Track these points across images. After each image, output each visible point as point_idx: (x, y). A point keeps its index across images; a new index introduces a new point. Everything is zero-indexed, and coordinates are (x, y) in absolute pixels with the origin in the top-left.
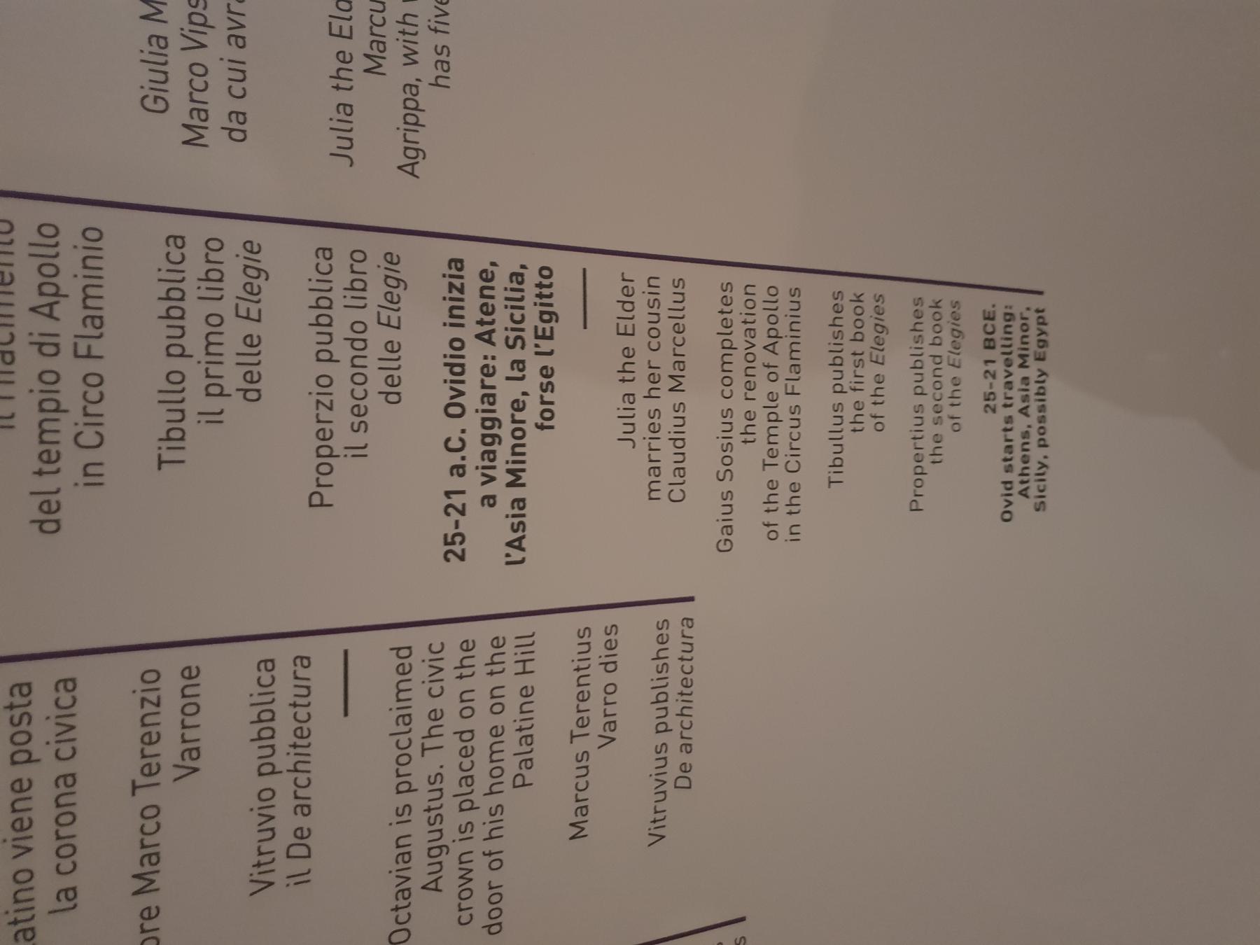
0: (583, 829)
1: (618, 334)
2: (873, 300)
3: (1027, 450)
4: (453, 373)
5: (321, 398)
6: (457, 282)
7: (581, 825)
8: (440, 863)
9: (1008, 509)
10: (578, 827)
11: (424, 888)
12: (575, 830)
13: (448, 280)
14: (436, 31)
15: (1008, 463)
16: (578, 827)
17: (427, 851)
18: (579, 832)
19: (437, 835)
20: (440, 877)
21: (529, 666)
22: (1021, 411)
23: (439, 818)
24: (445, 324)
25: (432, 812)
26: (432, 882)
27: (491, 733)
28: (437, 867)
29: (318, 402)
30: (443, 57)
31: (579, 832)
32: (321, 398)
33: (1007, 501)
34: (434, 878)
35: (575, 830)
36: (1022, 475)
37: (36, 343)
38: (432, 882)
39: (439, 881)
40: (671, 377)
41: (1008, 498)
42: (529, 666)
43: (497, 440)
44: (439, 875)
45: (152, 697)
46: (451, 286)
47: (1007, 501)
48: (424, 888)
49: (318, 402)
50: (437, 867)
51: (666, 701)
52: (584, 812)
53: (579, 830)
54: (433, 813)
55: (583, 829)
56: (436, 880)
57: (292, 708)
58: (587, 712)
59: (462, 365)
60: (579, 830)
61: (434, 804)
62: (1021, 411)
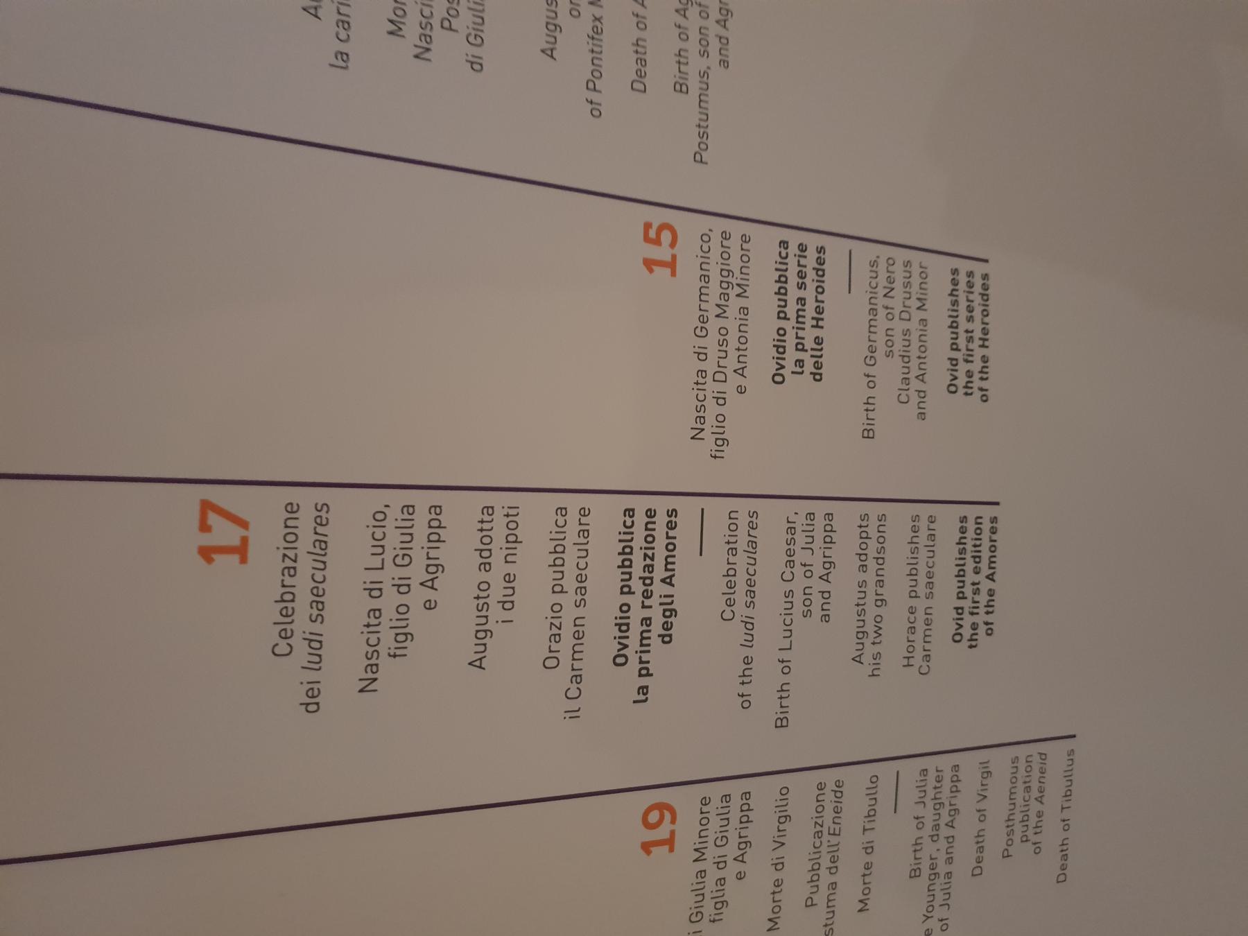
0: (704, 854)
1: (829, 834)
2: (902, 266)
3: (981, 523)
4: (620, 631)
5: (287, 552)
6: (650, 553)
7: (702, 850)
8: (485, 645)
9: (953, 382)
10: (700, 852)
11: (422, 584)
12: (697, 855)
13: (643, 551)
14: (715, 457)
15: (970, 335)
16: (700, 852)
17: (475, 633)
18: (701, 856)
19: (484, 621)
20: (485, 657)
21: (820, 323)
22: (987, 577)
23: (485, 606)
24: (476, 65)
25: (480, 600)
26: (429, 580)
27: (574, 636)
28: (482, 648)
29: (551, 623)
30: (701, 414)
31: (701, 856)
32: (287, 552)
33: (957, 624)
34: (430, 578)
35: (697, 855)
36: (971, 640)
37: (368, 589)
38: (429, 580)
39: (483, 660)
40: (718, 306)
41: (959, 622)
42: (820, 323)
43: (674, 613)
44: (483, 655)
45: (291, 554)
46: (646, 555)
47: (957, 624)
48: (422, 584)
49: (551, 623)
50: (482, 648)
51: (740, 843)
52: (722, 883)
53: (701, 854)
54: (481, 601)
55: (704, 854)
56: (481, 659)
57: (476, 600)
58: (718, 813)
59: (628, 625)
60: (701, 854)
61: (861, 602)
62: (987, 577)
